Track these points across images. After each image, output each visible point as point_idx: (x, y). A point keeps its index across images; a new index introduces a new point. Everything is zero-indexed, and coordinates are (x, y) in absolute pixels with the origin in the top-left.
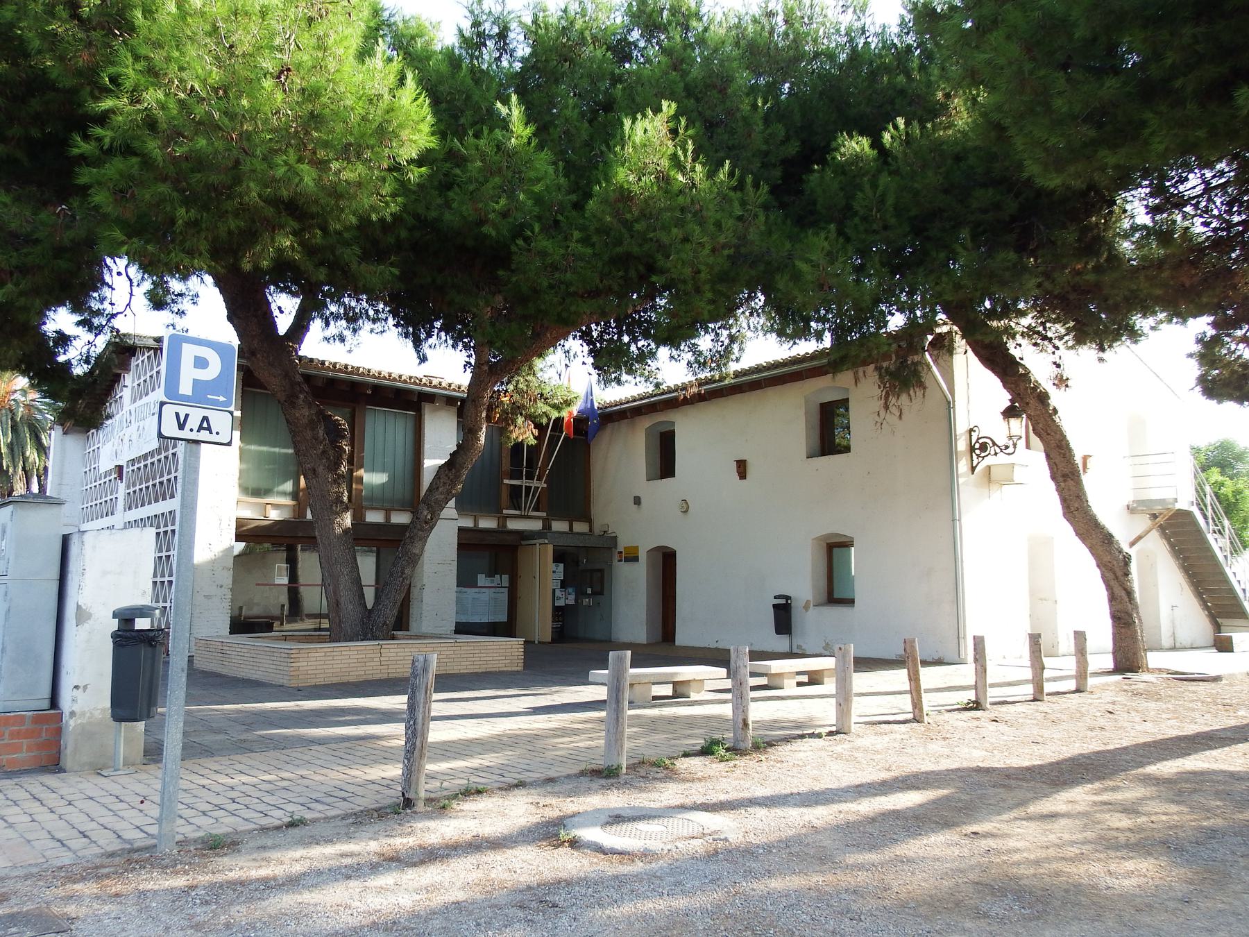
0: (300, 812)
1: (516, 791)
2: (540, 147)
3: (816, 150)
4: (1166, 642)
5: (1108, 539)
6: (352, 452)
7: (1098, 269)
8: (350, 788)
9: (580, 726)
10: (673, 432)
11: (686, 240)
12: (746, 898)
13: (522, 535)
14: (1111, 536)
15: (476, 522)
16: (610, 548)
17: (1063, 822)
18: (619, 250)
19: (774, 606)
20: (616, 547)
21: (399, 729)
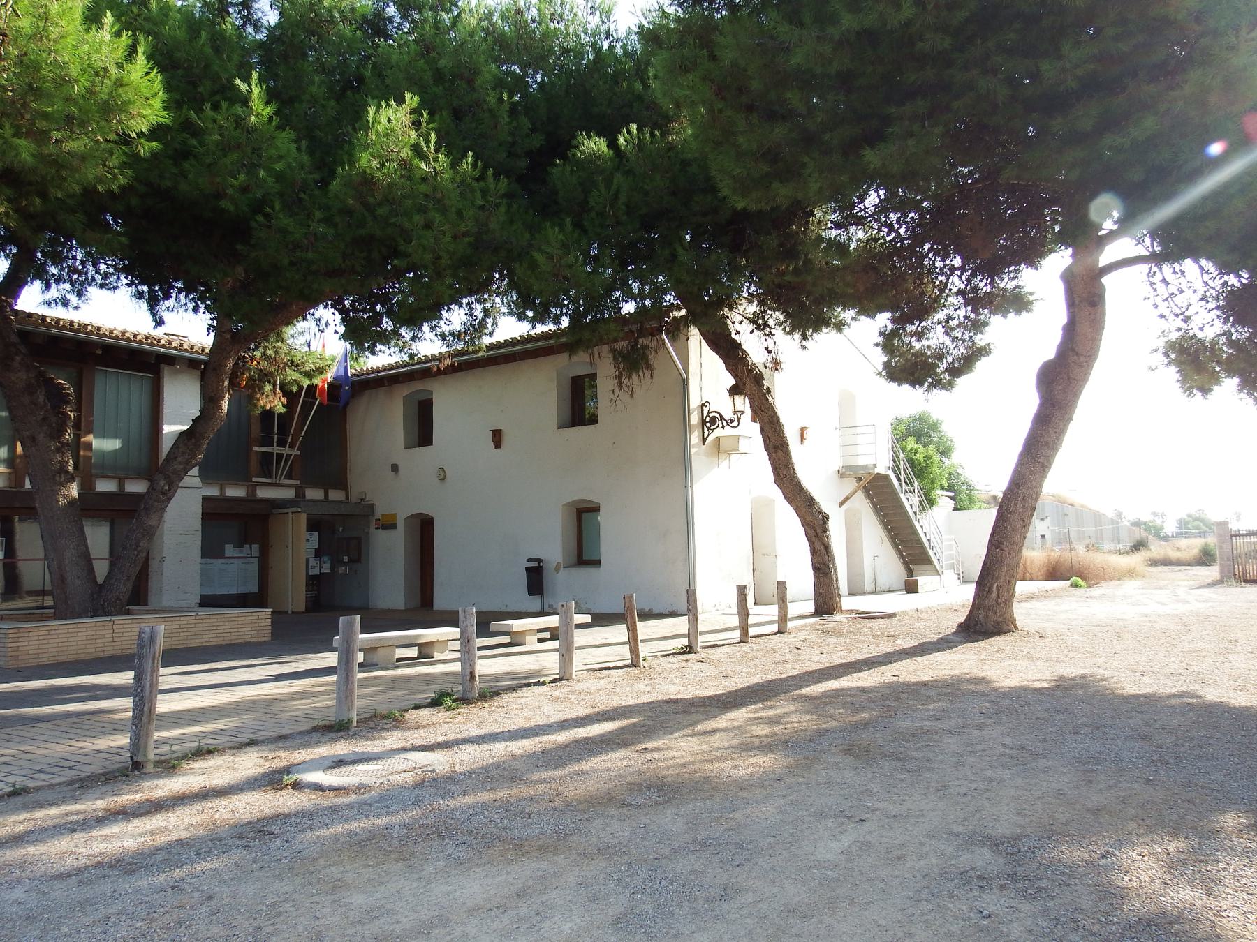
0: (21, 782)
1: (248, 749)
2: (280, 127)
3: (561, 146)
4: (868, 587)
5: (810, 501)
6: (78, 419)
7: (796, 272)
8: (73, 758)
9: (320, 689)
10: (431, 400)
11: (428, 226)
12: (440, 812)
14: (813, 499)
17: (719, 735)
18: (362, 232)
19: (527, 569)
21: (127, 702)
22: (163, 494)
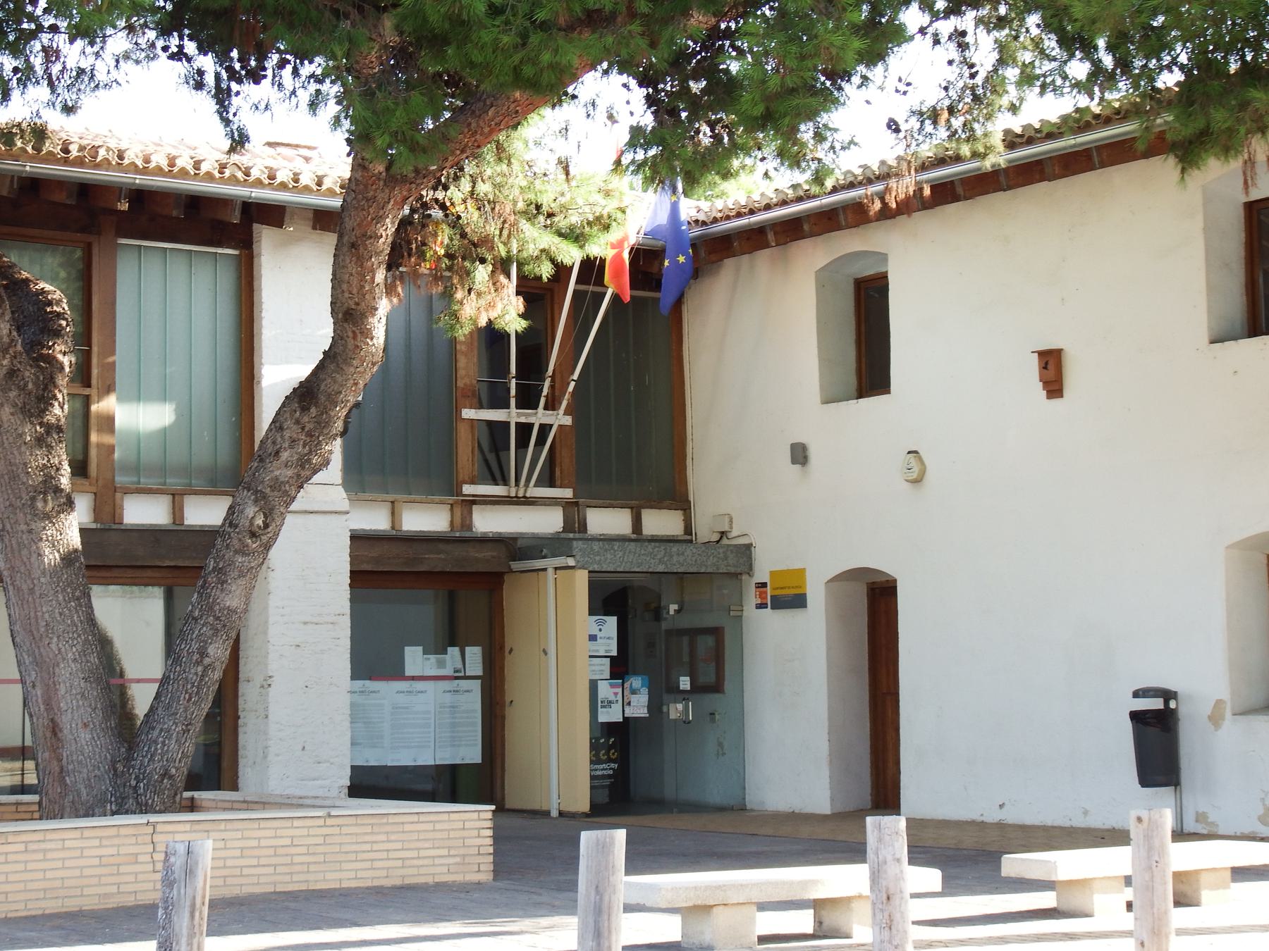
10: (884, 277)
13: (514, 548)
16: (736, 576)
19: (1136, 716)
20: (750, 570)
22: (253, 535)
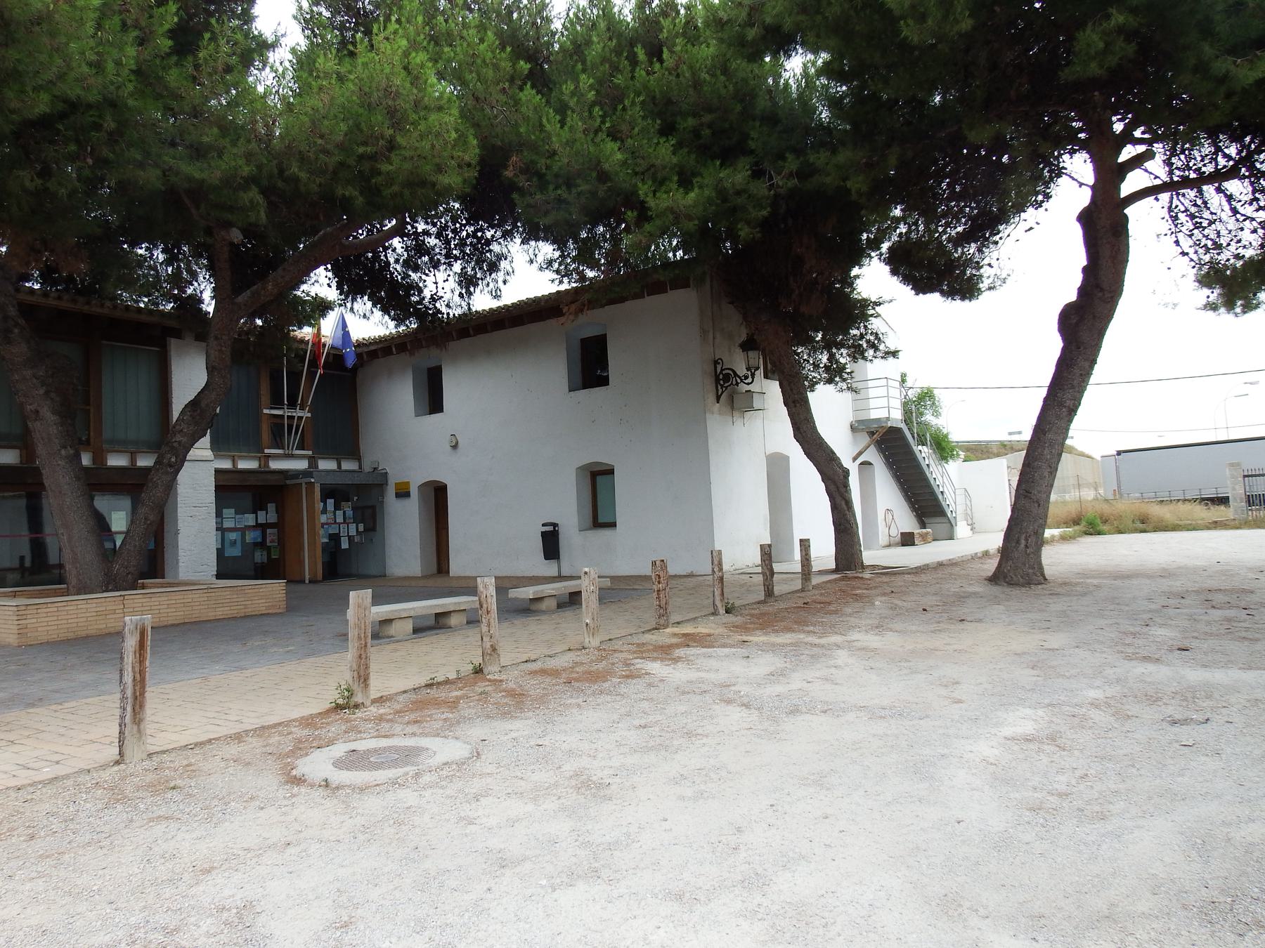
15: (234, 463)
22: (171, 466)
